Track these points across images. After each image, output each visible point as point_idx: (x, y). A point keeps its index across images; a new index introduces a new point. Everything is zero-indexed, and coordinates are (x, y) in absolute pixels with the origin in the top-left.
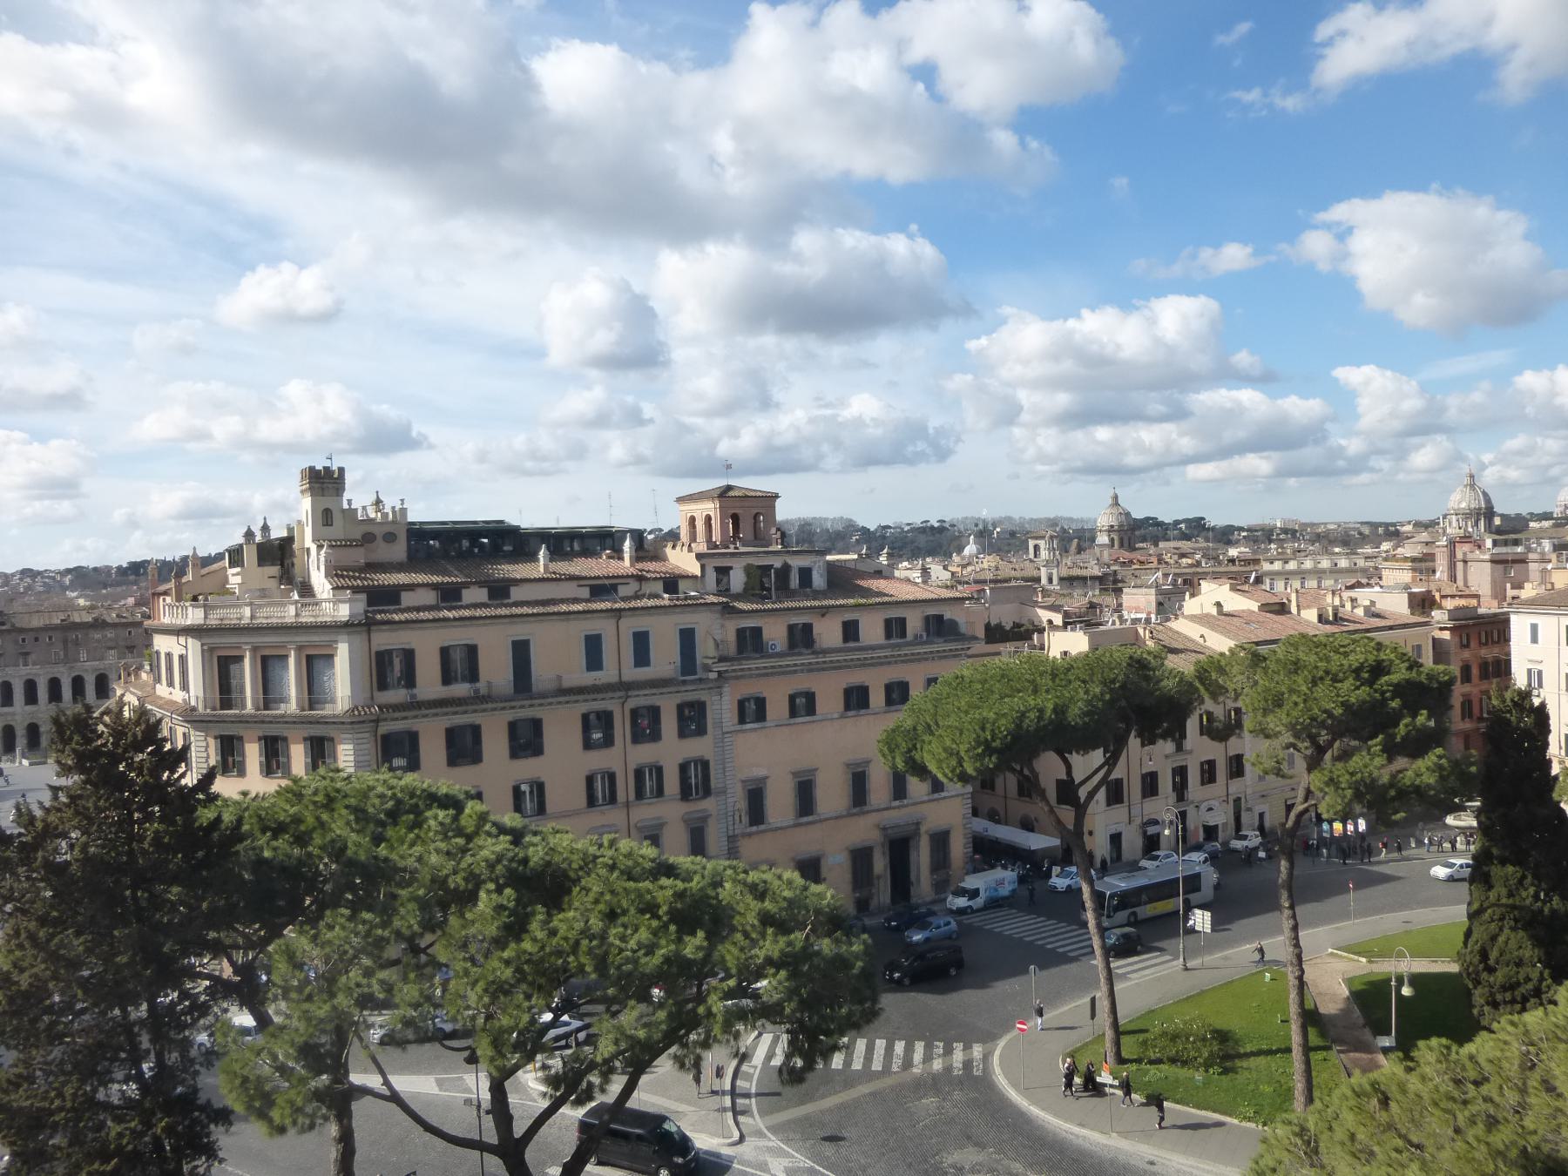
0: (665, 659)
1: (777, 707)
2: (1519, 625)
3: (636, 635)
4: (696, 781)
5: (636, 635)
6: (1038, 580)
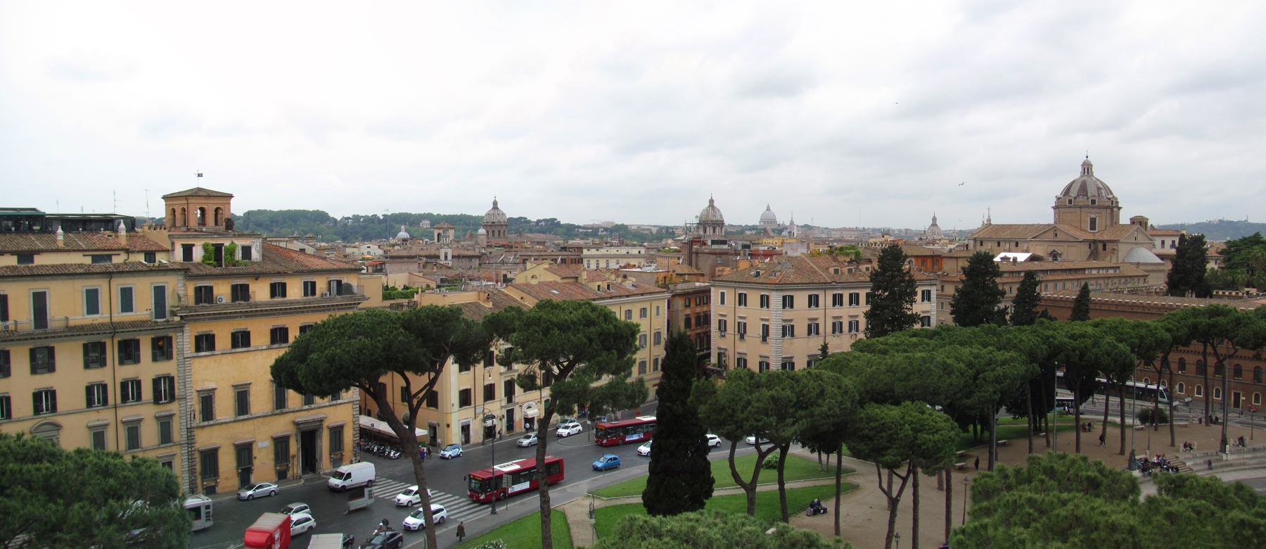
0: (143, 308)
1: (223, 341)
2: (715, 295)
3: (122, 290)
4: (165, 390)
5: (122, 290)
6: (438, 257)
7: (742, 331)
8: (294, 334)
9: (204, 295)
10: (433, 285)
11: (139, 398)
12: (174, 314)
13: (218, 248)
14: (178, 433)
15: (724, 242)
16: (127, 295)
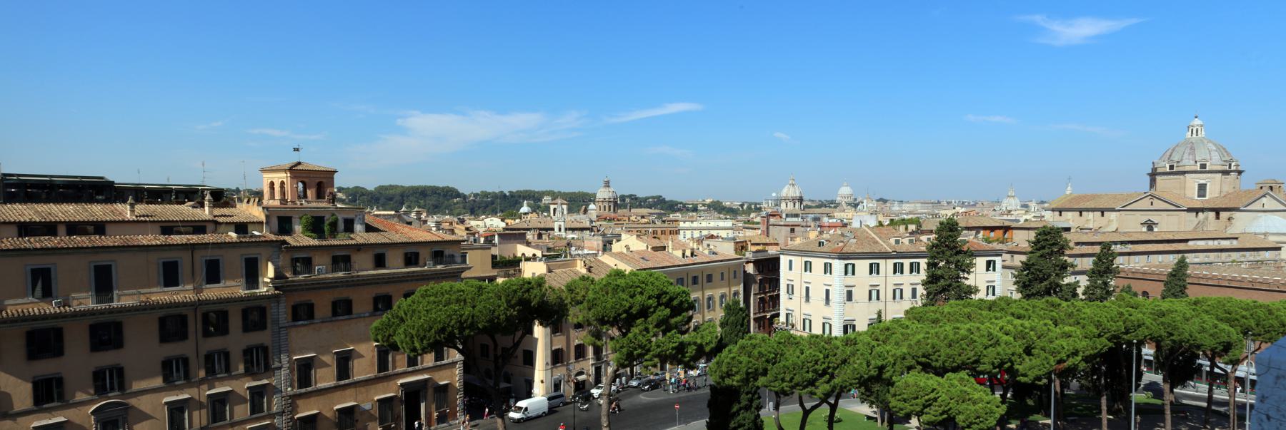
10: (539, 254)
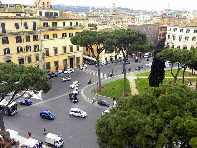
0: (30, 27)
1: (51, 37)
4: (37, 48)
7: (174, 38)
8: (74, 35)
9: (46, 25)
10: (100, 24)
11: (31, 50)
12: (38, 29)
13: (48, 13)
14: (40, 59)
15: (172, 15)
16: (26, 25)
